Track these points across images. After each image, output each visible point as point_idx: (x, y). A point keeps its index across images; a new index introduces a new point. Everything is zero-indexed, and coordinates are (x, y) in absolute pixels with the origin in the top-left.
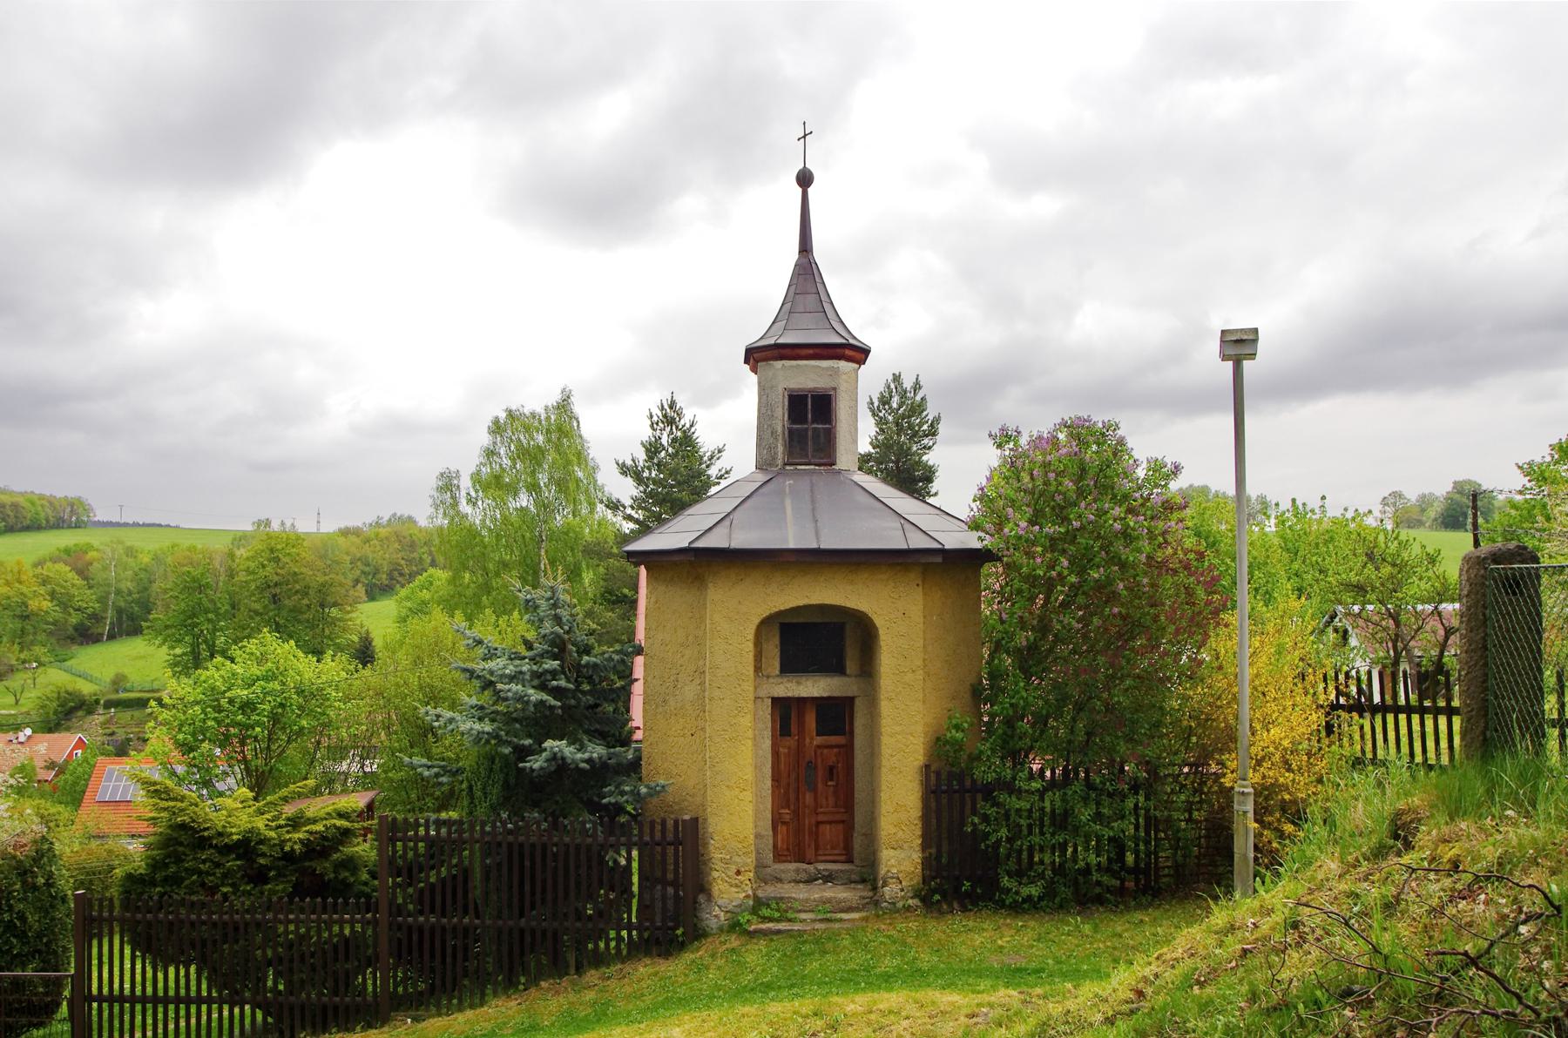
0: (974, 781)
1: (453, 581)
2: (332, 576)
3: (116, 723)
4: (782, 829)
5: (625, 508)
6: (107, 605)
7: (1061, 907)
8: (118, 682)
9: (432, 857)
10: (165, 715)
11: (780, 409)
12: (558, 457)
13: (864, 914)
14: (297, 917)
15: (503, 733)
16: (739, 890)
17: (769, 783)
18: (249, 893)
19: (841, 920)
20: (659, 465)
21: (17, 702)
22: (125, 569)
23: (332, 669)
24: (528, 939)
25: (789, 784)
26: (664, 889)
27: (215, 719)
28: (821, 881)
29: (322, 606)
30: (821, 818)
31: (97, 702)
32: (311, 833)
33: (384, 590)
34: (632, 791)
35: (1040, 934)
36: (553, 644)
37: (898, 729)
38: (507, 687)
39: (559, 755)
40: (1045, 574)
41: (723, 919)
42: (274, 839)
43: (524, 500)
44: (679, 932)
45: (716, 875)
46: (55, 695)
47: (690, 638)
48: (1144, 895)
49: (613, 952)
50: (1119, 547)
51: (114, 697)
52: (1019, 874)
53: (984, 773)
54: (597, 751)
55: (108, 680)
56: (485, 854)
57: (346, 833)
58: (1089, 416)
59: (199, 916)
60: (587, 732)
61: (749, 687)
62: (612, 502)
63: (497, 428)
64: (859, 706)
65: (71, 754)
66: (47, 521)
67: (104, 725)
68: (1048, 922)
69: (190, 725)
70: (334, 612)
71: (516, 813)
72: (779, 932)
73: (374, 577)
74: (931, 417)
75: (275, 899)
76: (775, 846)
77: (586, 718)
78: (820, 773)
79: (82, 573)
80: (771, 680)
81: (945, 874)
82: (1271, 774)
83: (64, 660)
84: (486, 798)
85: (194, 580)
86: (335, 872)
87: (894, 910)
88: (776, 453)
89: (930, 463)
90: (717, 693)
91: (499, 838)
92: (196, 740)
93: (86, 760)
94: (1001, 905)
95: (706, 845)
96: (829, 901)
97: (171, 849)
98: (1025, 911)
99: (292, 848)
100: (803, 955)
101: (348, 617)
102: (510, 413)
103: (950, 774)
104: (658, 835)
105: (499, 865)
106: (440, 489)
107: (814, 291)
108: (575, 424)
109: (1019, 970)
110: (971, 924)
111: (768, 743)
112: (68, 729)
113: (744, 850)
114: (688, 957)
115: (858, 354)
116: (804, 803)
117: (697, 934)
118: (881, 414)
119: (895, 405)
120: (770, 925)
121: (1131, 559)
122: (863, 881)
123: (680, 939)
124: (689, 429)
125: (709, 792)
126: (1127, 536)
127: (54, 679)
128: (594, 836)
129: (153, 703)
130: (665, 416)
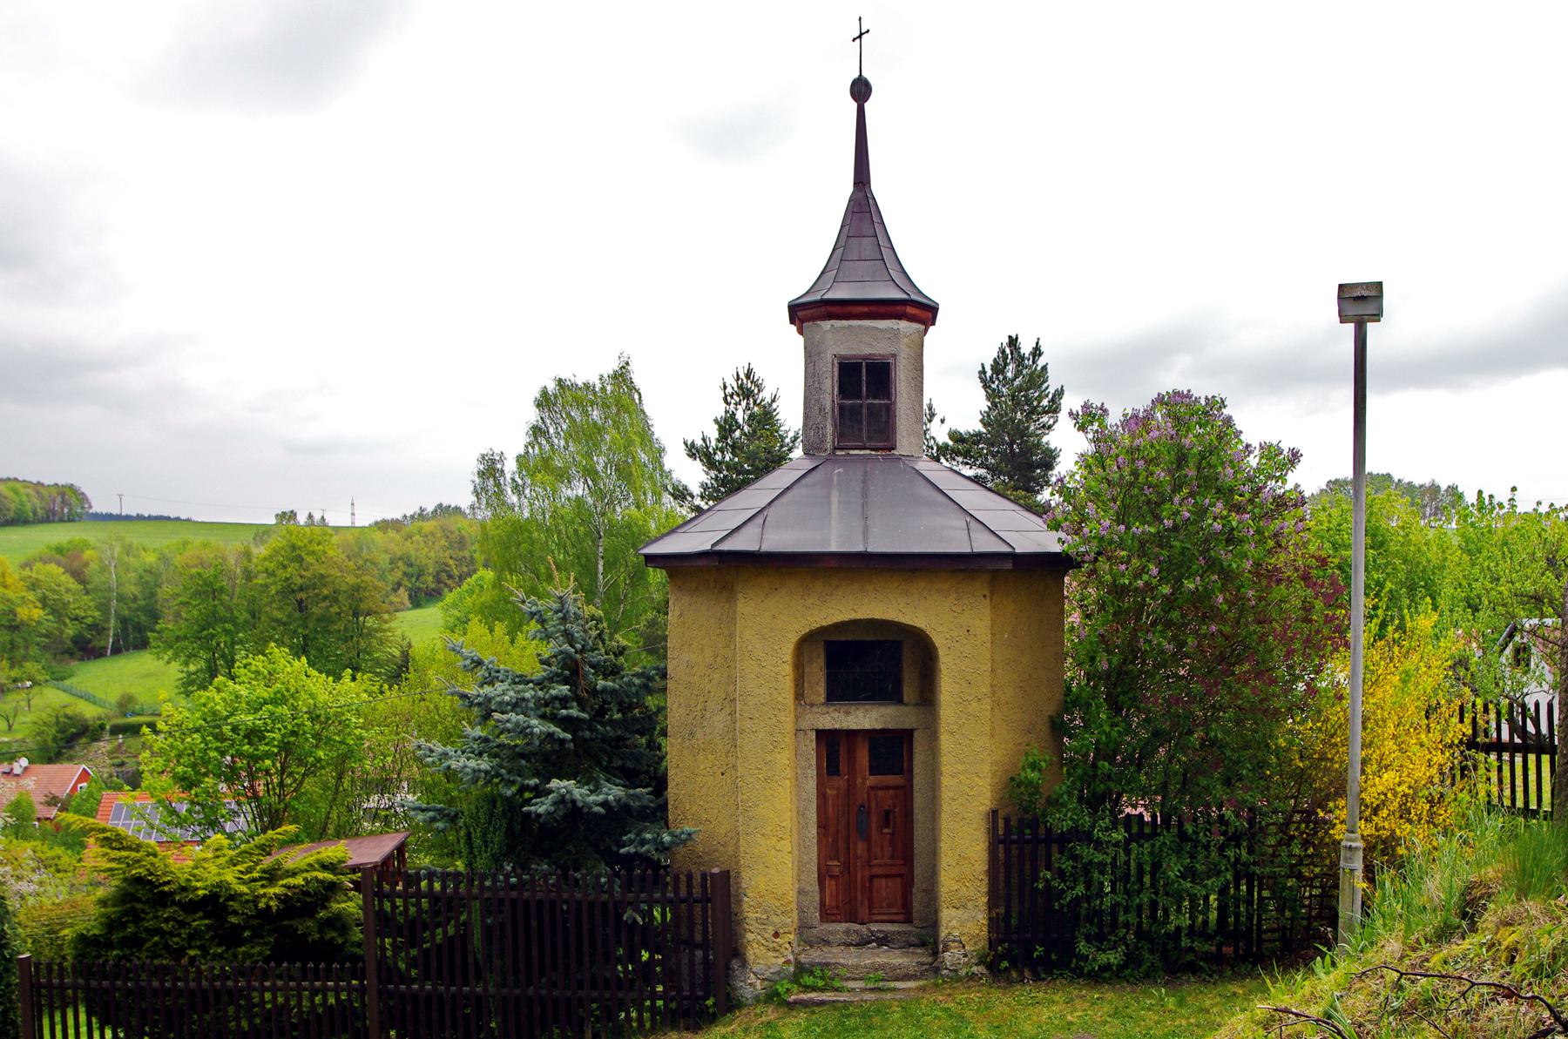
0: (1049, 831)
1: (498, 584)
3: (126, 751)
4: (830, 884)
5: (693, 497)
6: (109, 613)
7: (1147, 976)
8: (125, 705)
9: (438, 913)
10: (160, 742)
12: (618, 436)
13: (921, 983)
14: (274, 984)
15: (503, 771)
18: (220, 956)
19: (894, 990)
20: (733, 447)
21: (10, 727)
22: (127, 570)
23: (351, 690)
25: (838, 831)
26: (692, 953)
27: (217, 749)
28: (874, 944)
29: (356, 614)
30: (875, 871)
31: (102, 727)
32: (288, 887)
33: (431, 595)
34: (655, 840)
35: (1117, 1008)
36: (564, 666)
37: (960, 767)
38: (505, 717)
39: (568, 796)
40: (1130, 583)
41: (759, 987)
42: (247, 894)
43: (579, 489)
44: (710, 1002)
45: (750, 936)
46: (54, 720)
48: (1243, 963)
49: (635, 1024)
50: (1222, 553)
51: (120, 721)
52: (1098, 940)
53: (1061, 821)
54: (613, 792)
55: (113, 701)
56: (485, 912)
57: (332, 887)
58: (1189, 391)
59: (162, 984)
60: (605, 770)
62: (679, 491)
63: (545, 401)
64: (918, 738)
65: (74, 788)
66: (35, 513)
67: (111, 754)
68: (1129, 993)
69: (189, 755)
70: (370, 622)
71: (523, 866)
72: (822, 1003)
73: (417, 579)
74: (1052, 390)
75: (248, 963)
76: (822, 903)
77: (606, 752)
78: (874, 819)
79: (78, 575)
80: (815, 709)
81: (1014, 937)
82: (1386, 825)
83: (63, 679)
84: (486, 847)
85: (207, 583)
86: (320, 932)
87: (955, 978)
88: (824, 435)
89: (1052, 446)
90: (748, 724)
91: (502, 894)
92: (197, 773)
93: (91, 795)
95: (739, 902)
96: (881, 967)
97: (128, 906)
98: (1105, 981)
99: (267, 904)
100: (847, 1030)
101: (386, 626)
102: (560, 382)
103: (1021, 821)
104: (683, 892)
105: (502, 925)
106: (481, 474)
107: (871, 232)
108: (636, 397)
111: (812, 784)
112: (70, 759)
115: (926, 313)
117: (730, 1005)
118: (994, 386)
119: (1010, 375)
120: (813, 995)
121: (1234, 566)
122: (923, 944)
124: (770, 405)
125: (742, 842)
126: (1231, 538)
127: (51, 700)
128: (611, 891)
129: (145, 730)
130: (741, 387)
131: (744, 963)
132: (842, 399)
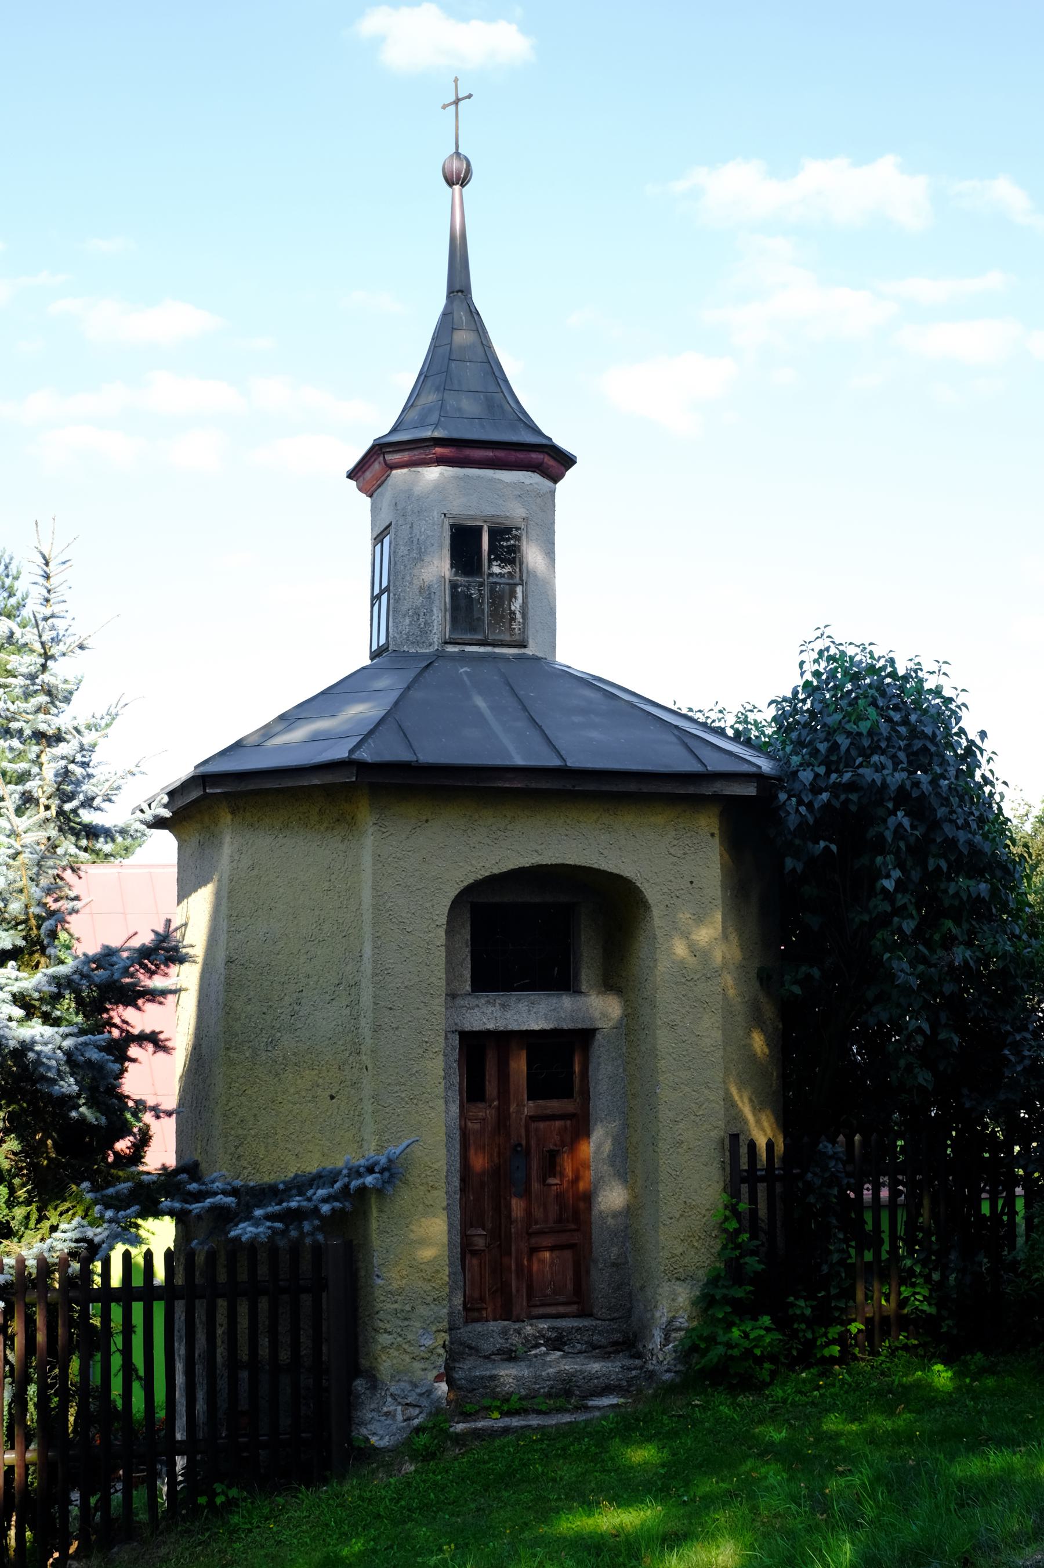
16: (427, 1365)
41: (400, 1417)
45: (384, 1339)
111: (455, 1109)
131: (374, 1383)
132: (456, 574)
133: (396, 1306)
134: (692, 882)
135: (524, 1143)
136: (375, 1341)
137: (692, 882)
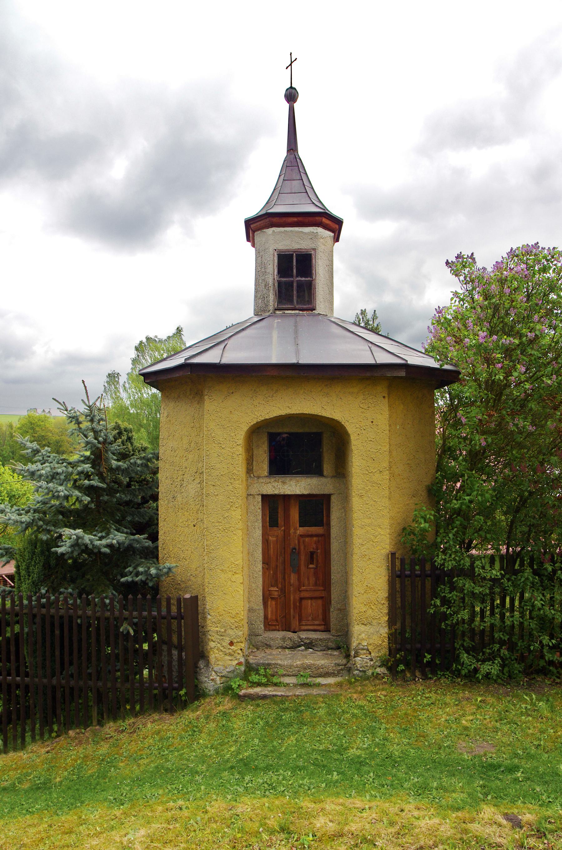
2: (63, 437)
11: (271, 266)
13: (338, 679)
17: (260, 566)
19: (319, 685)
24: (59, 695)
28: (303, 648)
30: (304, 594)
34: (146, 572)
37: (367, 521)
41: (219, 682)
44: (182, 692)
45: (212, 644)
47: (192, 444)
61: (240, 486)
71: (54, 589)
72: (264, 697)
76: (266, 617)
78: (303, 557)
80: (261, 480)
81: (408, 646)
84: (29, 576)
88: (268, 301)
91: (35, 611)
94: (457, 674)
96: (309, 667)
109: (493, 767)
110: (433, 696)
111: (258, 533)
113: (236, 624)
114: (189, 715)
116: (290, 582)
122: (338, 648)
123: (183, 698)
128: (112, 610)
133: (217, 629)
134: (372, 422)
135: (297, 548)
136: (207, 644)
137: (372, 422)
